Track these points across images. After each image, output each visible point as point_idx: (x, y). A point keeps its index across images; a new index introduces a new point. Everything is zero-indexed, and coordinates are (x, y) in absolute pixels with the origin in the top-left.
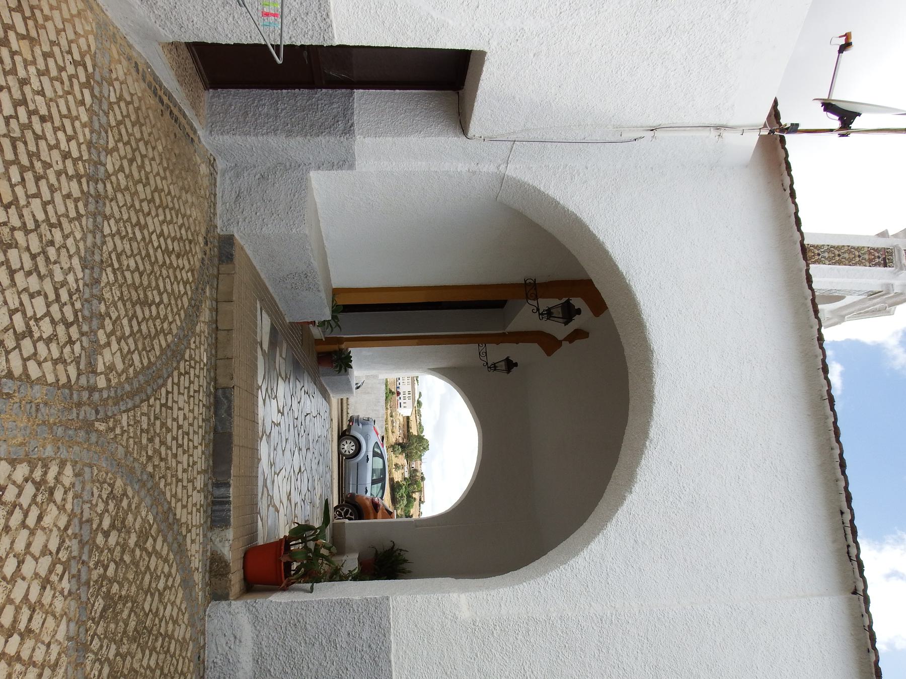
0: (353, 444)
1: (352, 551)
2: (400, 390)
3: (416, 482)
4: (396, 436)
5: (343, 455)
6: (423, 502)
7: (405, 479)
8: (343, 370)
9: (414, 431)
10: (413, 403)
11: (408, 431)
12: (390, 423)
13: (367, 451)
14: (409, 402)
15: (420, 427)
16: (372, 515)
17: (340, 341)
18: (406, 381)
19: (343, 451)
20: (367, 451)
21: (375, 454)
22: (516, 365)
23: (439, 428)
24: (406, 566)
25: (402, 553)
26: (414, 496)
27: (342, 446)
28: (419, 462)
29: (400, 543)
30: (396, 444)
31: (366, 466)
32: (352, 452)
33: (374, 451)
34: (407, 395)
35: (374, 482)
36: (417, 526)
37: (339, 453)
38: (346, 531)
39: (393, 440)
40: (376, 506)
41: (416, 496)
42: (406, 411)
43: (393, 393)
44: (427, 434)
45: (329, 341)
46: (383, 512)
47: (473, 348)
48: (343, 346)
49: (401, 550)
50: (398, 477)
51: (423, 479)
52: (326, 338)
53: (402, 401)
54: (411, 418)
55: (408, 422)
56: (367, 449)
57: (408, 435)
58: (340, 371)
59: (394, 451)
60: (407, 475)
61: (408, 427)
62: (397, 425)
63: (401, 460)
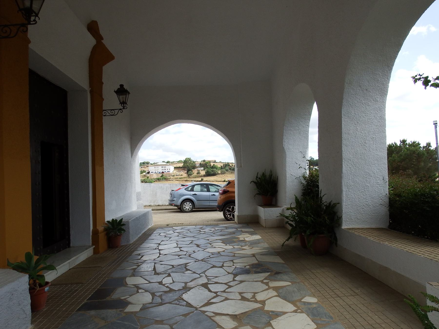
0: (185, 204)
1: (256, 210)
2: (161, 172)
3: (206, 164)
4: (183, 174)
5: (192, 208)
6: (215, 161)
7: (204, 169)
8: (123, 227)
9: (181, 165)
10: (168, 165)
11: (181, 168)
12: (177, 177)
13: (190, 195)
14: (167, 167)
15: (180, 162)
16: (232, 194)
17: (95, 233)
18: (157, 169)
19: (190, 209)
20: (190, 195)
21: (192, 190)
22: (122, 86)
23: (179, 152)
24: (268, 174)
25: (259, 176)
26: (212, 165)
27: (187, 210)
28: (196, 163)
29: (252, 177)
30: (187, 174)
31: (199, 195)
32: (190, 204)
33: (190, 191)
34: (164, 168)
35: (208, 191)
36: (241, 166)
37: (192, 211)
38: (243, 214)
39: (185, 175)
40: (225, 192)
41: (212, 164)
42: (171, 169)
43: (163, 175)
44: (183, 159)
45: (95, 241)
46: (229, 188)
47: (107, 121)
48: (100, 228)
49: (257, 177)
50: (203, 173)
51: (204, 161)
52: (93, 244)
53: (166, 171)
54: (175, 166)
55: (177, 168)
56: (189, 195)
57: (183, 168)
58: (124, 230)
59: (191, 175)
60: (202, 168)
61: (179, 168)
62: (178, 173)
63: (195, 171)
